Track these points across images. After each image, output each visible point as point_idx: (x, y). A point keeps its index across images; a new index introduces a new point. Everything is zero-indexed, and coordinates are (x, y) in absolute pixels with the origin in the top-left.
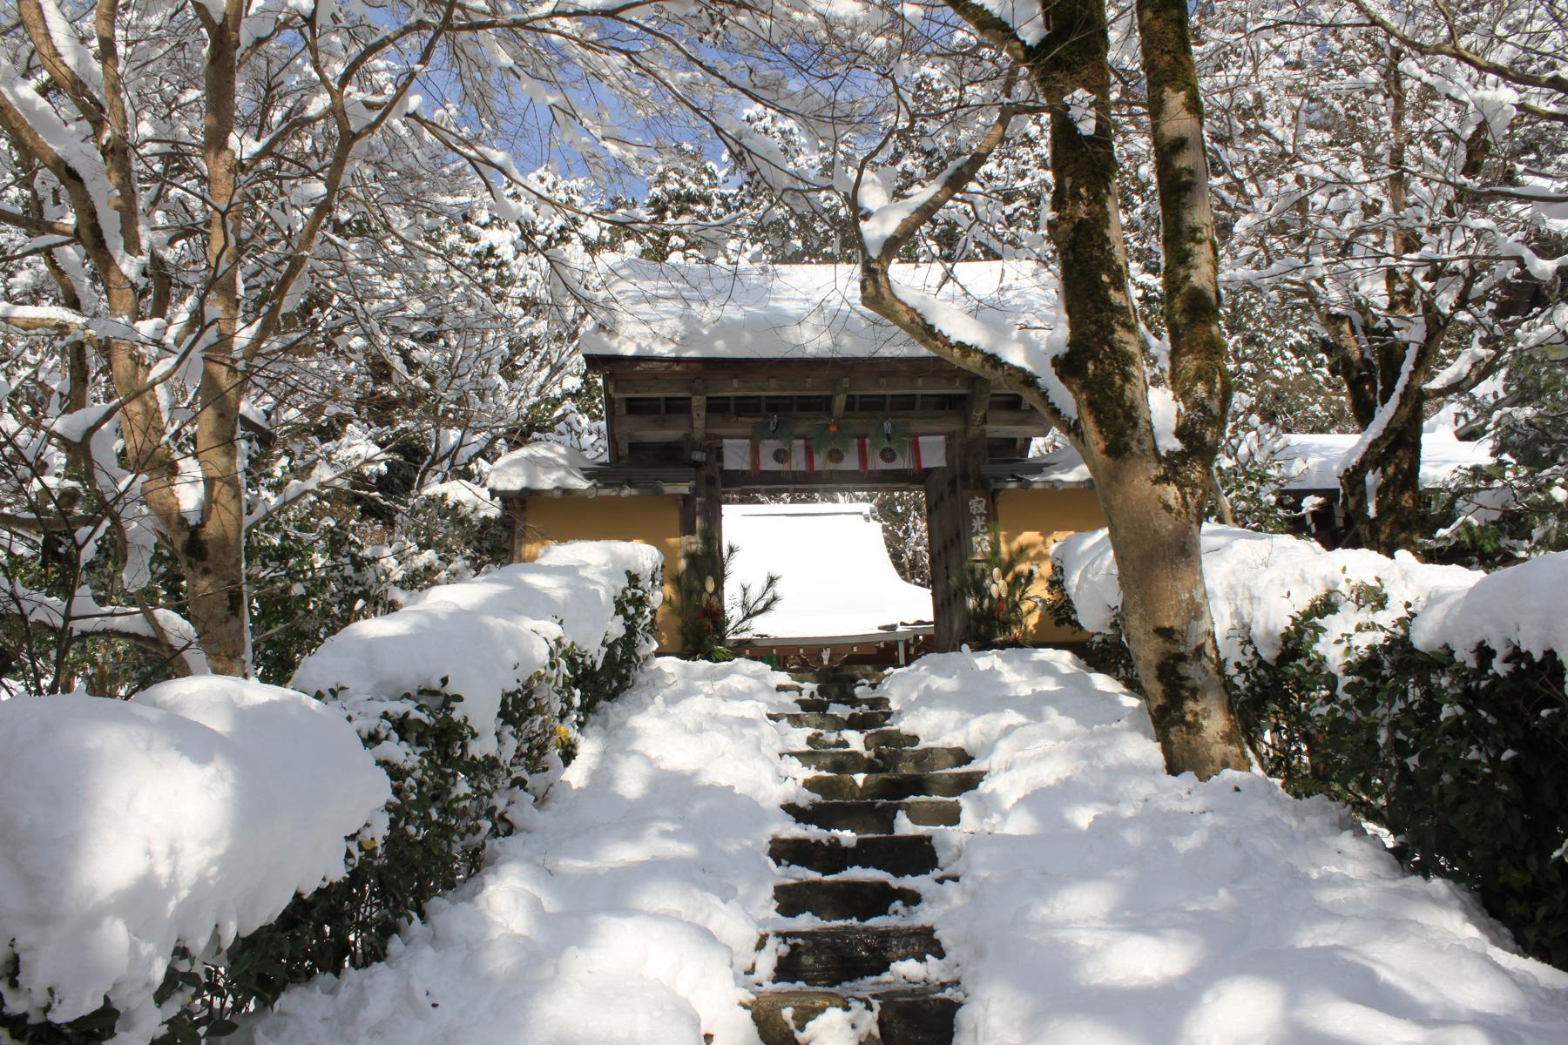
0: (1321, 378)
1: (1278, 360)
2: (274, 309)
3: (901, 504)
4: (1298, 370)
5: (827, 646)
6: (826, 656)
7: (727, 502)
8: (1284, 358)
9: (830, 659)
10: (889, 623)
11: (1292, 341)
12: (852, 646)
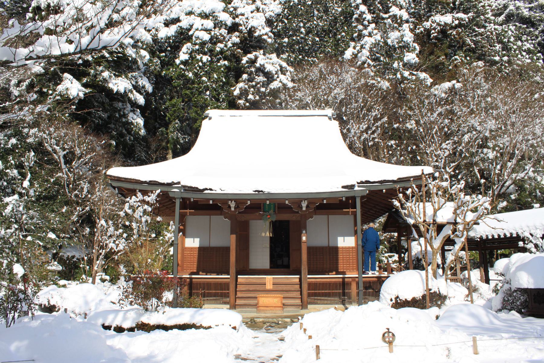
0: (540, 65)
1: (519, 56)
2: (429, 243)
3: (346, 116)
4: (529, 61)
5: (305, 199)
6: (304, 204)
7: (352, 248)
8: (522, 55)
9: (307, 207)
10: (349, 183)
11: (526, 48)
12: (323, 199)
